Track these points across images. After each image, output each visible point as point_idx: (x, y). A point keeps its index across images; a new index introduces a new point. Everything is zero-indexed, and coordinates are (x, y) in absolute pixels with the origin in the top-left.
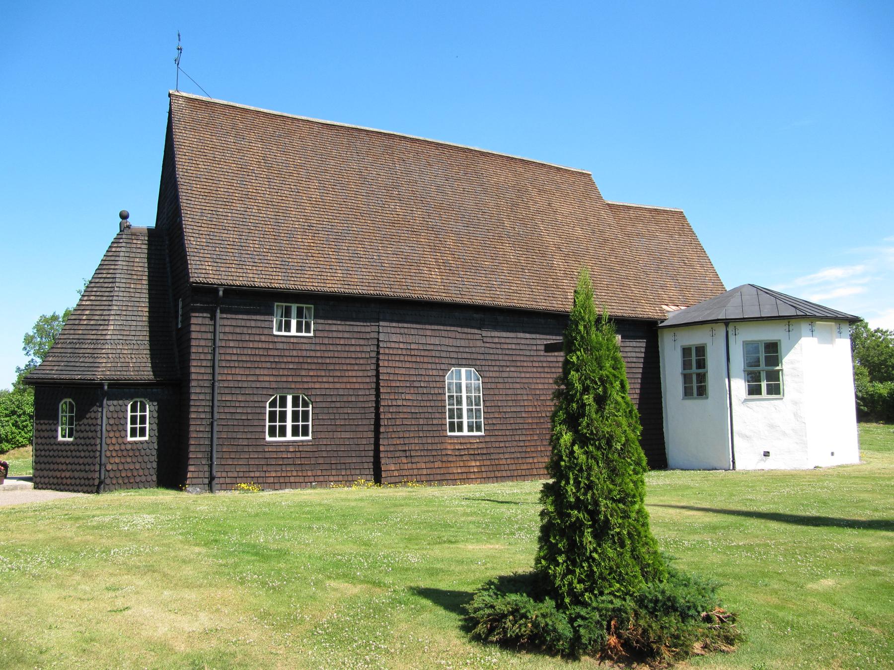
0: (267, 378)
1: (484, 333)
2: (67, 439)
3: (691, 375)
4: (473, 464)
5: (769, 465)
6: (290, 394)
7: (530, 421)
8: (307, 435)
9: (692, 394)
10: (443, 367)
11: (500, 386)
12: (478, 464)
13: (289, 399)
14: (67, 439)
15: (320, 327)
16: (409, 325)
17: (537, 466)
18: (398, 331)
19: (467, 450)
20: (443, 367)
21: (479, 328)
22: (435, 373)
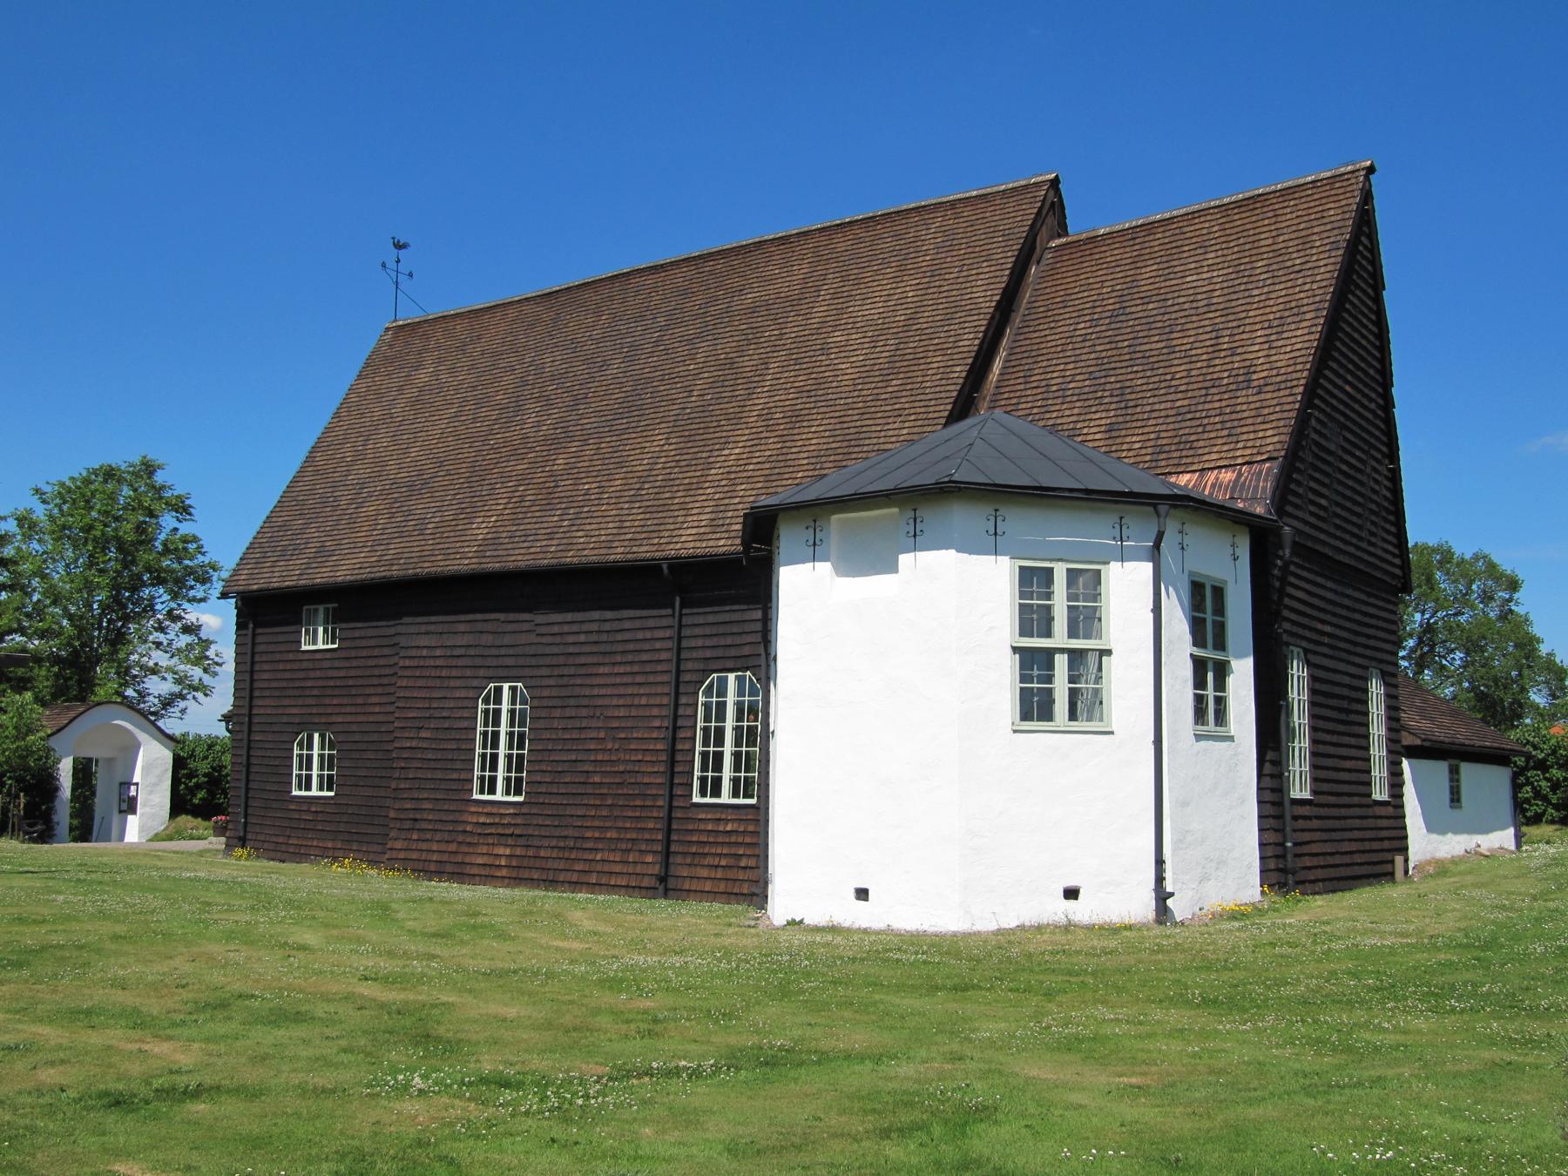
0: (295, 711)
1: (540, 619)
2: (326, 793)
3: (1049, 654)
4: (501, 851)
5: (1080, 912)
6: (133, 851)
7: (597, 779)
8: (752, 797)
9: (1046, 714)
10: (475, 683)
11: (557, 713)
12: (508, 852)
13: (316, 736)
14: (326, 793)
15: (349, 634)
16: (441, 618)
17: (599, 868)
18: (423, 629)
19: (499, 825)
20: (475, 683)
21: (530, 611)
22: (463, 693)
